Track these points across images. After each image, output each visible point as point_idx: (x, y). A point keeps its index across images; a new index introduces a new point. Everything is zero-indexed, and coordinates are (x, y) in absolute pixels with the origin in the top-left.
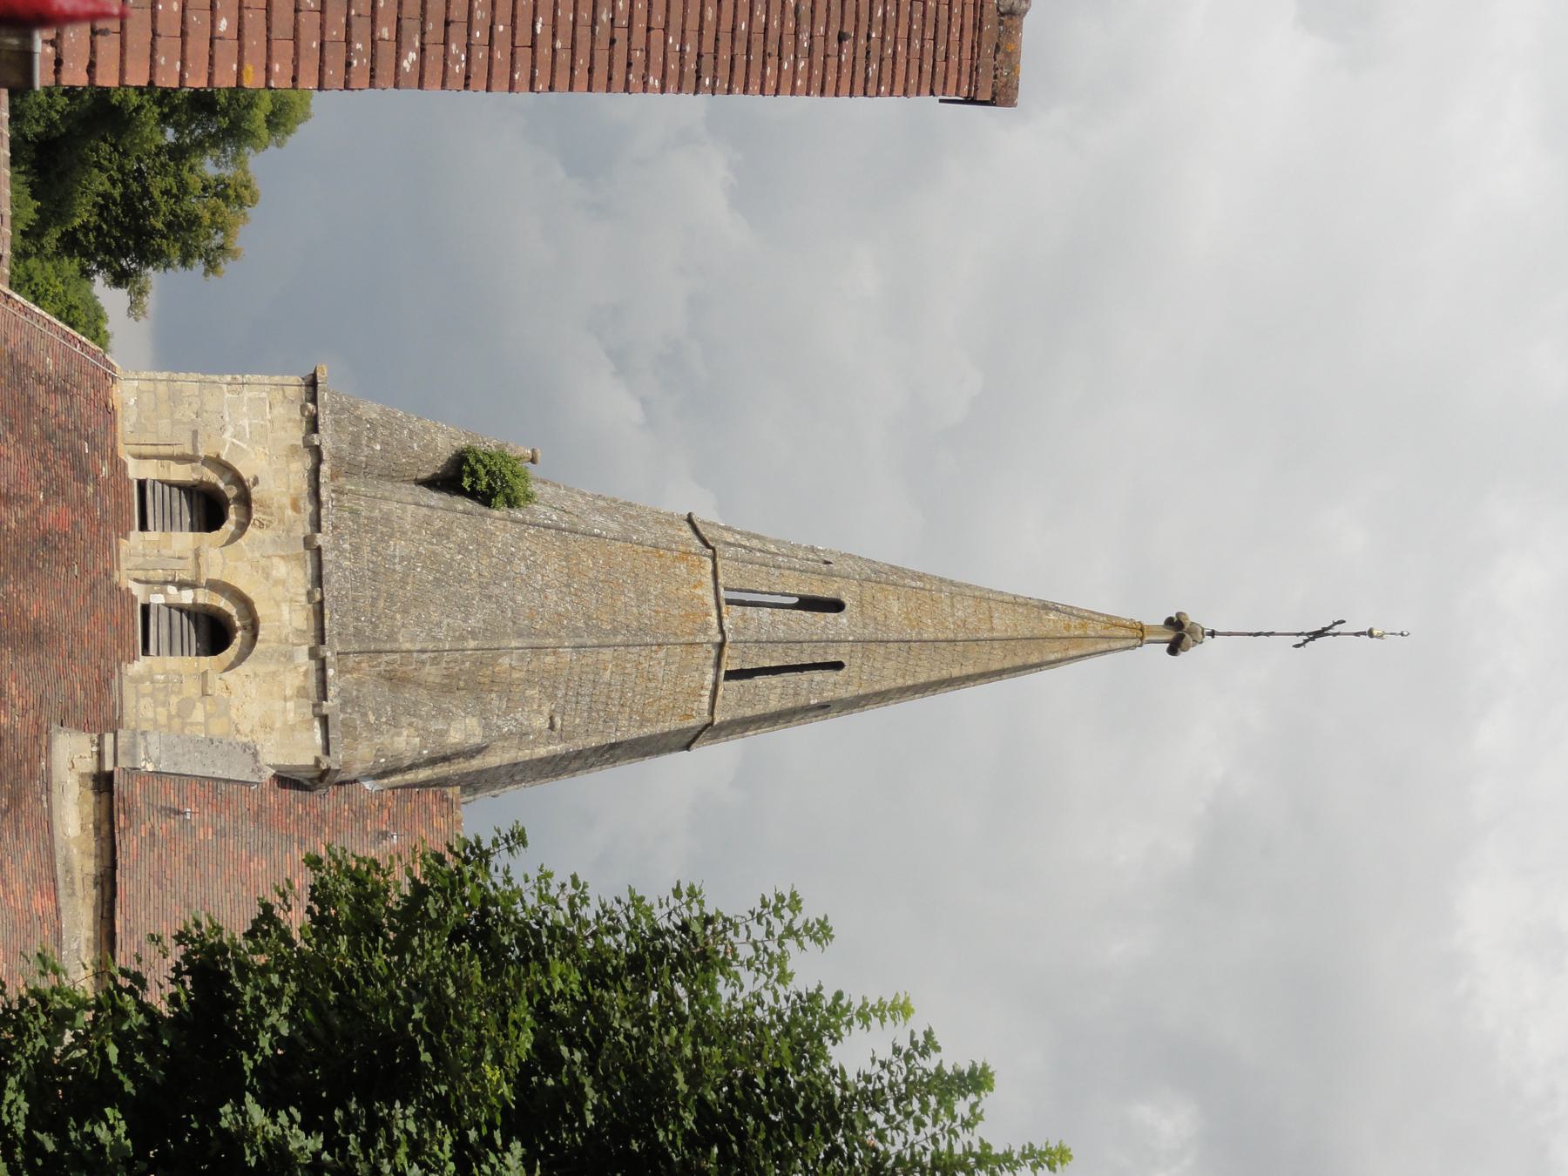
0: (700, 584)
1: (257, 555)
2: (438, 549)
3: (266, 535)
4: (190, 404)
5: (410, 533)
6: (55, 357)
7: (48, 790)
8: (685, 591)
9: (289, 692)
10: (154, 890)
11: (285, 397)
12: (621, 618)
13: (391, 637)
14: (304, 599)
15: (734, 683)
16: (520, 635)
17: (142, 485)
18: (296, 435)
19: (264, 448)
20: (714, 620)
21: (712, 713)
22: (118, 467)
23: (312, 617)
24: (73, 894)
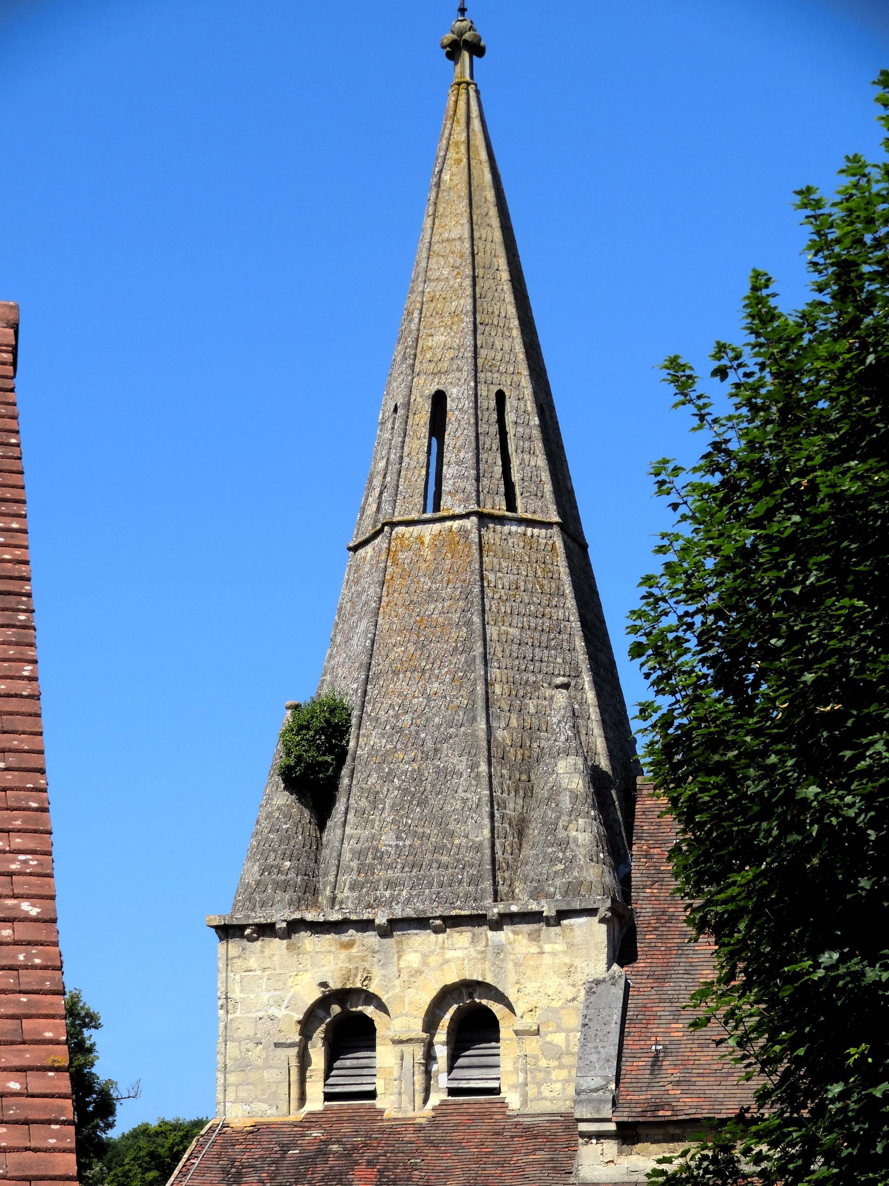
0: (420, 539)
1: (397, 982)
3: (377, 973)
4: (248, 1050)
5: (373, 831)
8: (427, 553)
9: (534, 949)
11: (239, 957)
12: (455, 617)
13: (478, 848)
15: (519, 503)
16: (474, 719)
17: (328, 1097)
18: (276, 946)
19: (290, 976)
20: (456, 524)
21: (548, 525)
22: (312, 1120)
23: (457, 929)
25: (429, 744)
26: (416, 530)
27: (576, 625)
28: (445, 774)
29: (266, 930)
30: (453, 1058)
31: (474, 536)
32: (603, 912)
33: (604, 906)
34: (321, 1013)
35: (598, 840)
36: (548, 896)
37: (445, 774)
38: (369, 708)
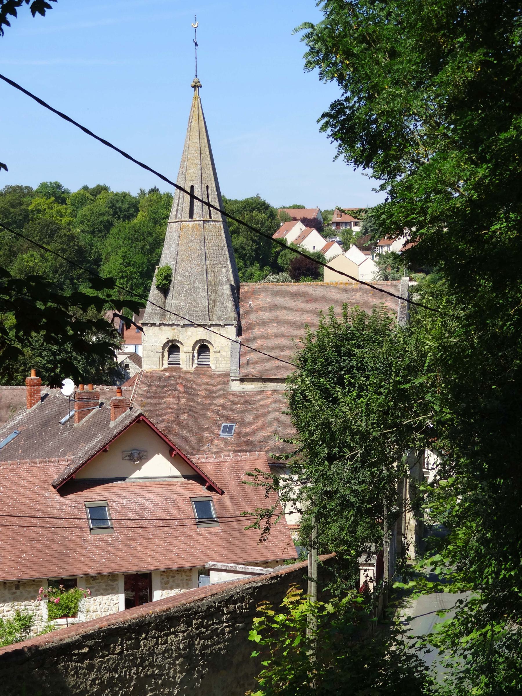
0: (188, 226)
3: (181, 336)
6: (142, 387)
7: (244, 392)
8: (190, 230)
10: (265, 368)
12: (198, 248)
13: (205, 307)
15: (212, 216)
16: (203, 275)
17: (169, 364)
20: (197, 222)
21: (219, 221)
22: (165, 370)
24: (267, 387)
25: (192, 280)
26: (187, 223)
27: (226, 248)
28: (196, 288)
29: (153, 325)
30: (199, 356)
31: (202, 226)
32: (235, 325)
33: (235, 323)
34: (167, 344)
35: (233, 306)
36: (222, 320)
37: (196, 288)
38: (177, 270)
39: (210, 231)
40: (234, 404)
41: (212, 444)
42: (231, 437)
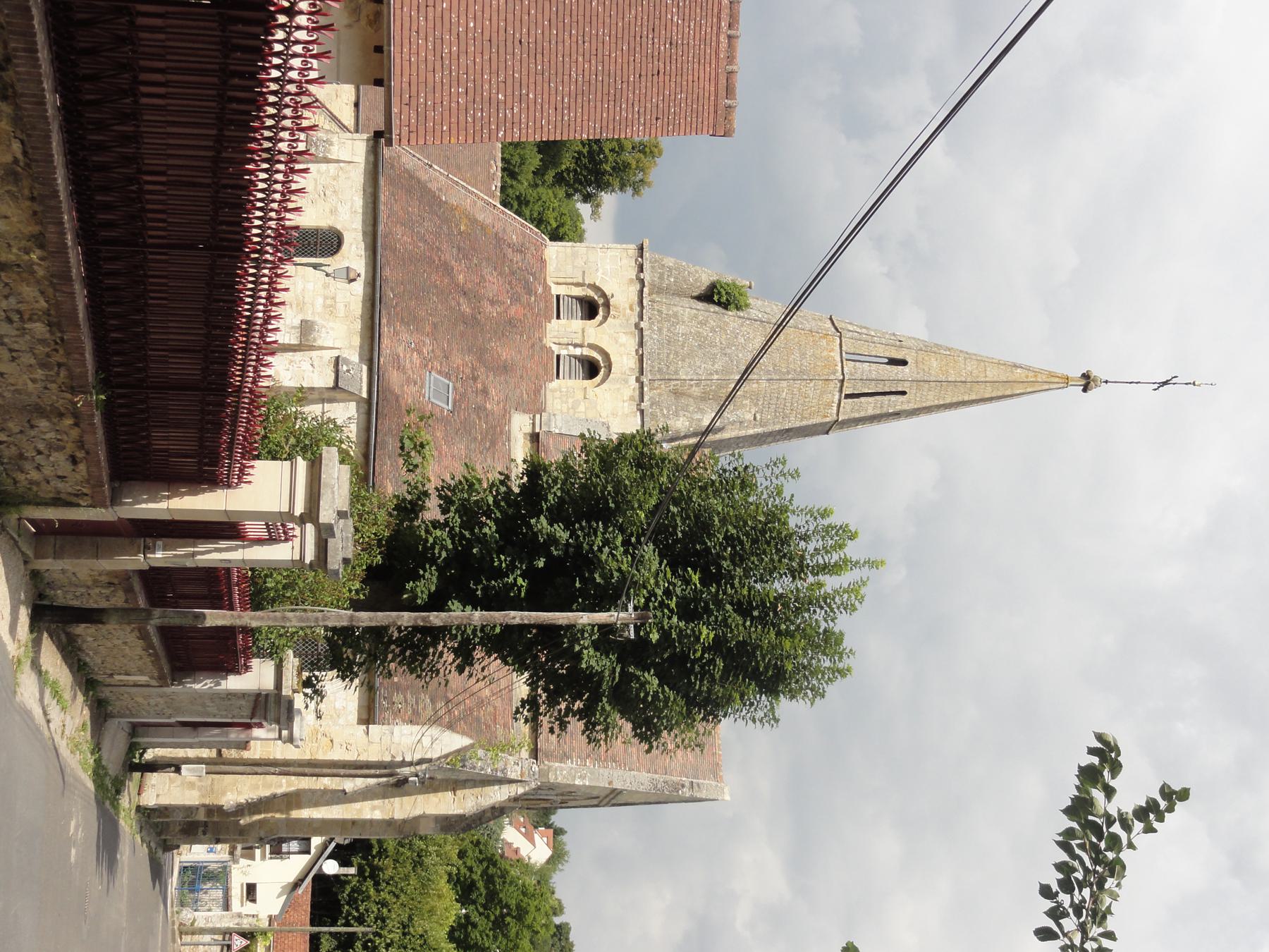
0: (832, 350)
2: (701, 330)
3: (617, 322)
6: (517, 235)
7: (509, 440)
8: (825, 353)
13: (676, 372)
14: (634, 353)
17: (558, 297)
20: (839, 368)
21: (838, 415)
22: (547, 288)
26: (838, 348)
28: (713, 359)
30: (575, 357)
37: (713, 359)
39: (823, 393)
40: (487, 415)
41: (413, 350)
42: (427, 395)
